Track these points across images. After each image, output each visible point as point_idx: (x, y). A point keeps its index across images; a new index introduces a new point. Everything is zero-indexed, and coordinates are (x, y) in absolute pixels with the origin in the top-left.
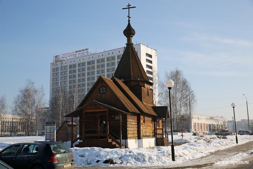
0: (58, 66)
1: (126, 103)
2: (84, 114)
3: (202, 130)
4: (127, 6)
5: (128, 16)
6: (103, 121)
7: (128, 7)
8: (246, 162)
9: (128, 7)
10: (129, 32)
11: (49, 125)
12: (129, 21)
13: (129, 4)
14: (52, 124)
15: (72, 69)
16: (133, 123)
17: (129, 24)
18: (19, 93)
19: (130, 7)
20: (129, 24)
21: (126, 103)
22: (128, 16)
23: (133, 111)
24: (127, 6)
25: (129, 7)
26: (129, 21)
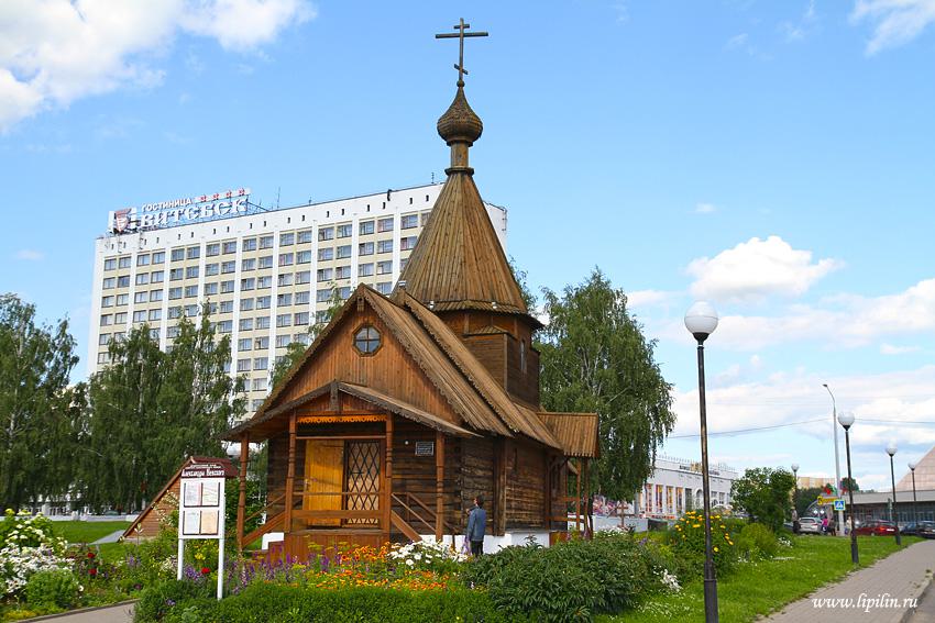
0: (125, 252)
1: (457, 393)
2: (292, 429)
3: (661, 510)
4: (456, 28)
5: (456, 66)
6: (40, 493)
7: (458, 31)
8: (908, 602)
9: (458, 31)
10: (461, 130)
11: (196, 474)
12: (461, 85)
13: (462, 20)
14: (211, 470)
15: (184, 264)
16: (480, 473)
17: (460, 99)
18: (655, 363)
19: (466, 31)
20: (460, 99)
21: (457, 393)
22: (456, 66)
23: (481, 418)
24: (456, 28)
25: (462, 33)
26: (461, 85)
